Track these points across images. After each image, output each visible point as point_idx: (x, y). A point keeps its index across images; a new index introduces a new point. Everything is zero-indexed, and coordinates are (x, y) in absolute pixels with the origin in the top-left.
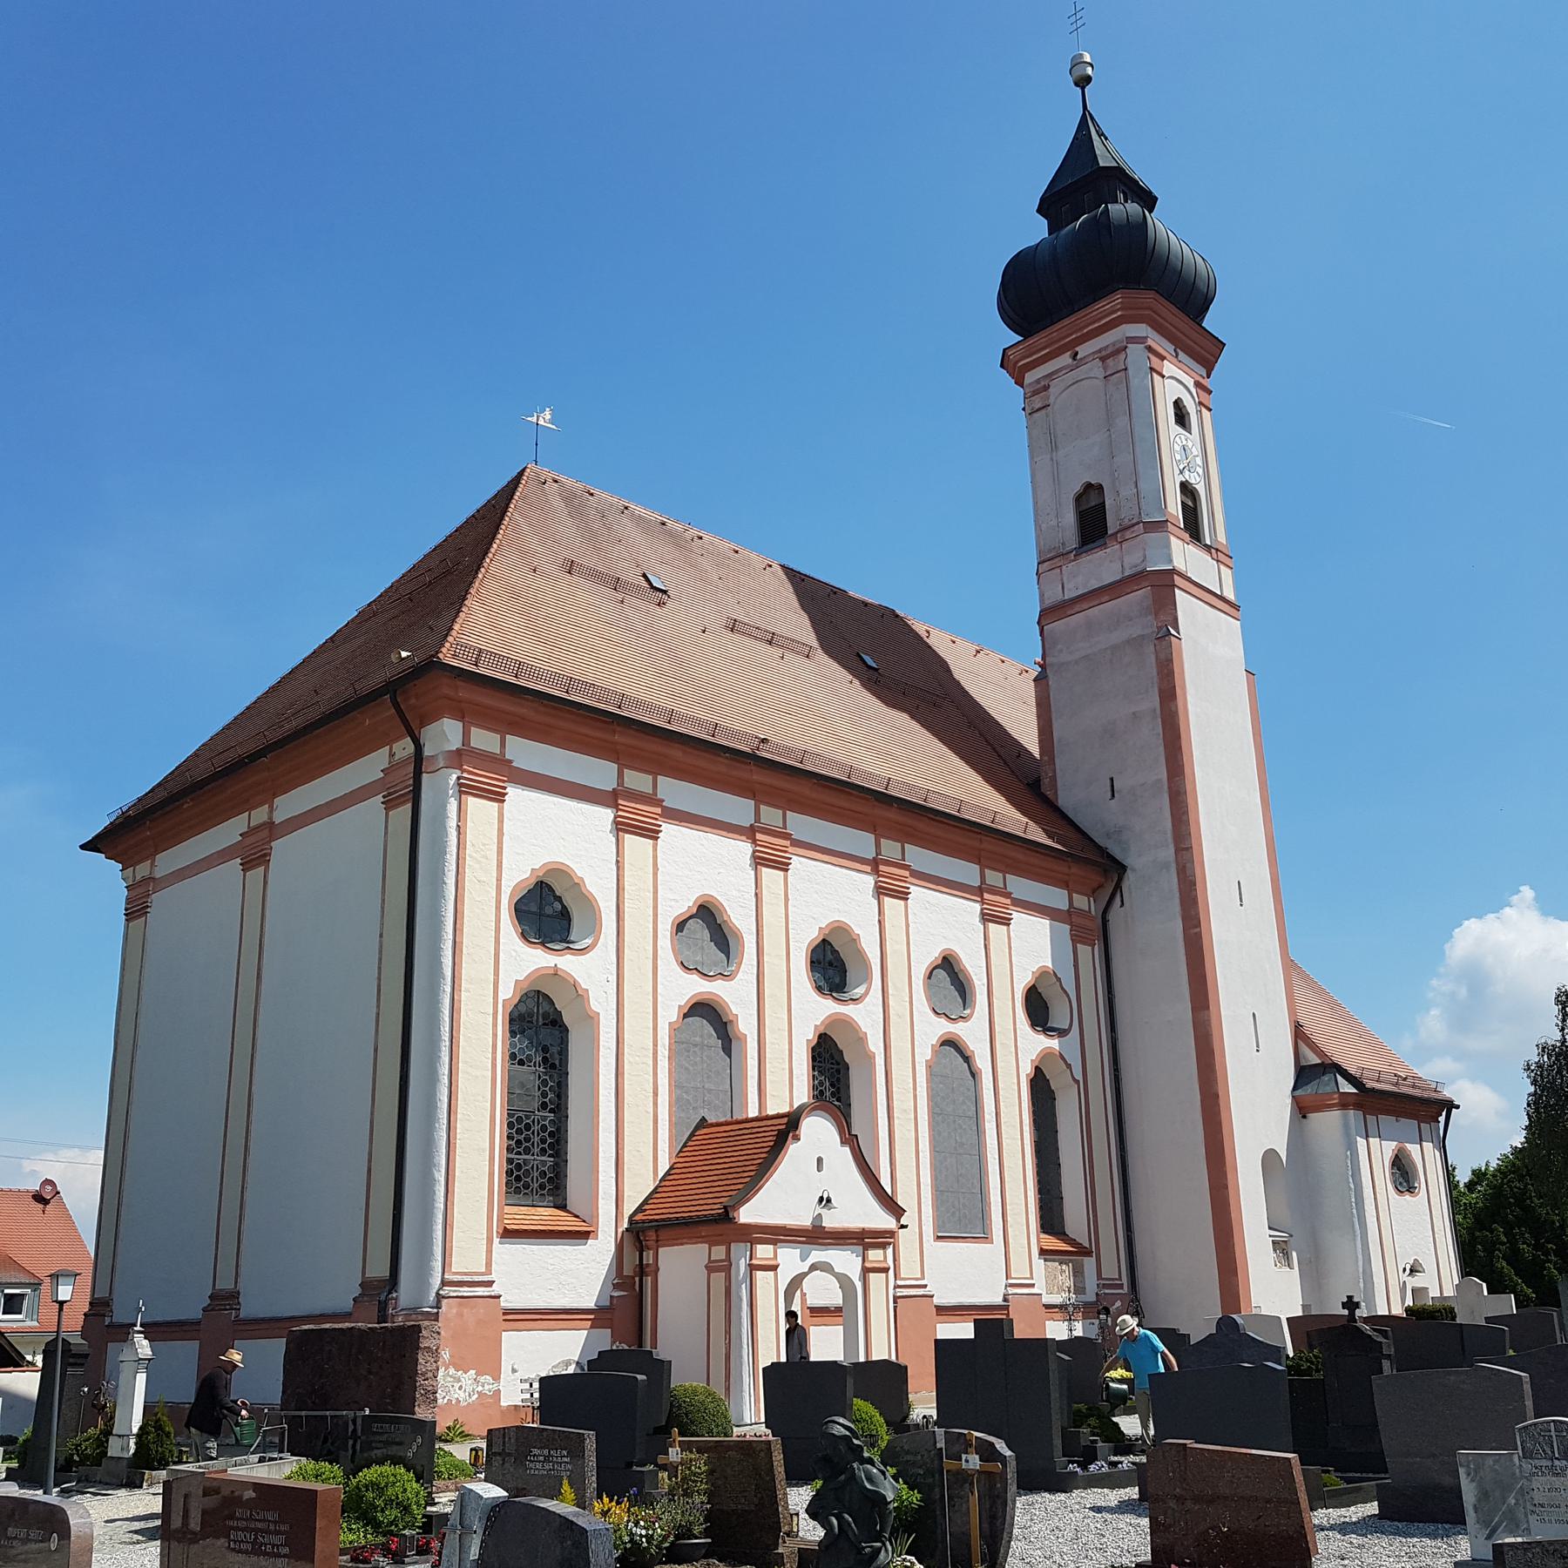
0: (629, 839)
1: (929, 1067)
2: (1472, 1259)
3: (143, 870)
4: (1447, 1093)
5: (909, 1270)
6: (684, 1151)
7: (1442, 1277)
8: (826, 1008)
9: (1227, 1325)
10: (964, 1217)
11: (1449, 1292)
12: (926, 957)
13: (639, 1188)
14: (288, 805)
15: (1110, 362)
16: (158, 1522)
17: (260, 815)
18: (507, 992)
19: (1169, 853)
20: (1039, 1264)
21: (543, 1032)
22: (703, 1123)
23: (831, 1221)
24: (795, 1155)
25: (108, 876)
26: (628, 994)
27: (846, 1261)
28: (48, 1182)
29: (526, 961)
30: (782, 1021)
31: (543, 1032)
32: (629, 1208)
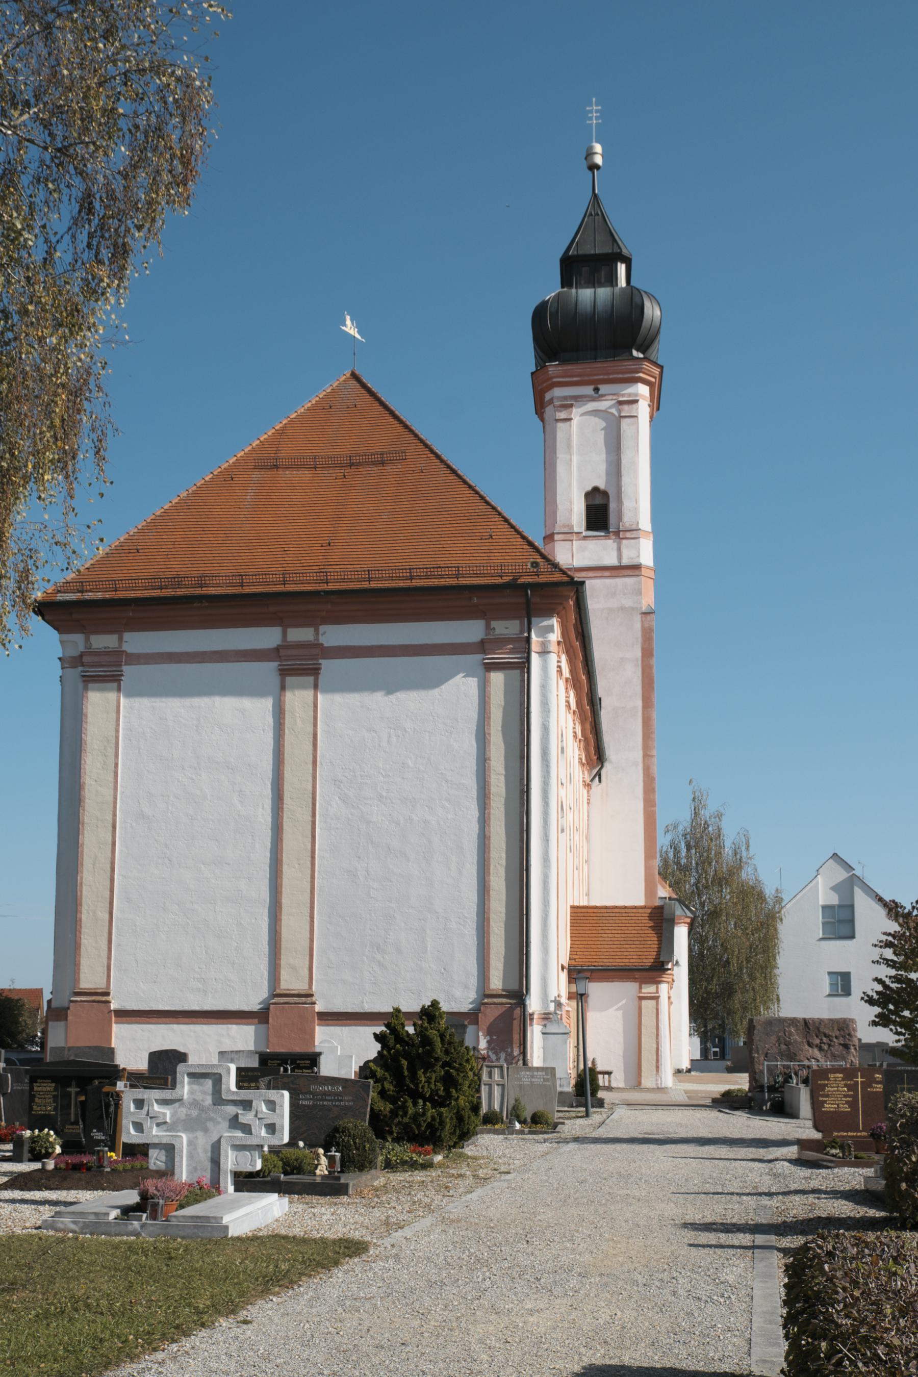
14: (334, 635)
15: (626, 407)
17: (300, 634)
19: (638, 755)
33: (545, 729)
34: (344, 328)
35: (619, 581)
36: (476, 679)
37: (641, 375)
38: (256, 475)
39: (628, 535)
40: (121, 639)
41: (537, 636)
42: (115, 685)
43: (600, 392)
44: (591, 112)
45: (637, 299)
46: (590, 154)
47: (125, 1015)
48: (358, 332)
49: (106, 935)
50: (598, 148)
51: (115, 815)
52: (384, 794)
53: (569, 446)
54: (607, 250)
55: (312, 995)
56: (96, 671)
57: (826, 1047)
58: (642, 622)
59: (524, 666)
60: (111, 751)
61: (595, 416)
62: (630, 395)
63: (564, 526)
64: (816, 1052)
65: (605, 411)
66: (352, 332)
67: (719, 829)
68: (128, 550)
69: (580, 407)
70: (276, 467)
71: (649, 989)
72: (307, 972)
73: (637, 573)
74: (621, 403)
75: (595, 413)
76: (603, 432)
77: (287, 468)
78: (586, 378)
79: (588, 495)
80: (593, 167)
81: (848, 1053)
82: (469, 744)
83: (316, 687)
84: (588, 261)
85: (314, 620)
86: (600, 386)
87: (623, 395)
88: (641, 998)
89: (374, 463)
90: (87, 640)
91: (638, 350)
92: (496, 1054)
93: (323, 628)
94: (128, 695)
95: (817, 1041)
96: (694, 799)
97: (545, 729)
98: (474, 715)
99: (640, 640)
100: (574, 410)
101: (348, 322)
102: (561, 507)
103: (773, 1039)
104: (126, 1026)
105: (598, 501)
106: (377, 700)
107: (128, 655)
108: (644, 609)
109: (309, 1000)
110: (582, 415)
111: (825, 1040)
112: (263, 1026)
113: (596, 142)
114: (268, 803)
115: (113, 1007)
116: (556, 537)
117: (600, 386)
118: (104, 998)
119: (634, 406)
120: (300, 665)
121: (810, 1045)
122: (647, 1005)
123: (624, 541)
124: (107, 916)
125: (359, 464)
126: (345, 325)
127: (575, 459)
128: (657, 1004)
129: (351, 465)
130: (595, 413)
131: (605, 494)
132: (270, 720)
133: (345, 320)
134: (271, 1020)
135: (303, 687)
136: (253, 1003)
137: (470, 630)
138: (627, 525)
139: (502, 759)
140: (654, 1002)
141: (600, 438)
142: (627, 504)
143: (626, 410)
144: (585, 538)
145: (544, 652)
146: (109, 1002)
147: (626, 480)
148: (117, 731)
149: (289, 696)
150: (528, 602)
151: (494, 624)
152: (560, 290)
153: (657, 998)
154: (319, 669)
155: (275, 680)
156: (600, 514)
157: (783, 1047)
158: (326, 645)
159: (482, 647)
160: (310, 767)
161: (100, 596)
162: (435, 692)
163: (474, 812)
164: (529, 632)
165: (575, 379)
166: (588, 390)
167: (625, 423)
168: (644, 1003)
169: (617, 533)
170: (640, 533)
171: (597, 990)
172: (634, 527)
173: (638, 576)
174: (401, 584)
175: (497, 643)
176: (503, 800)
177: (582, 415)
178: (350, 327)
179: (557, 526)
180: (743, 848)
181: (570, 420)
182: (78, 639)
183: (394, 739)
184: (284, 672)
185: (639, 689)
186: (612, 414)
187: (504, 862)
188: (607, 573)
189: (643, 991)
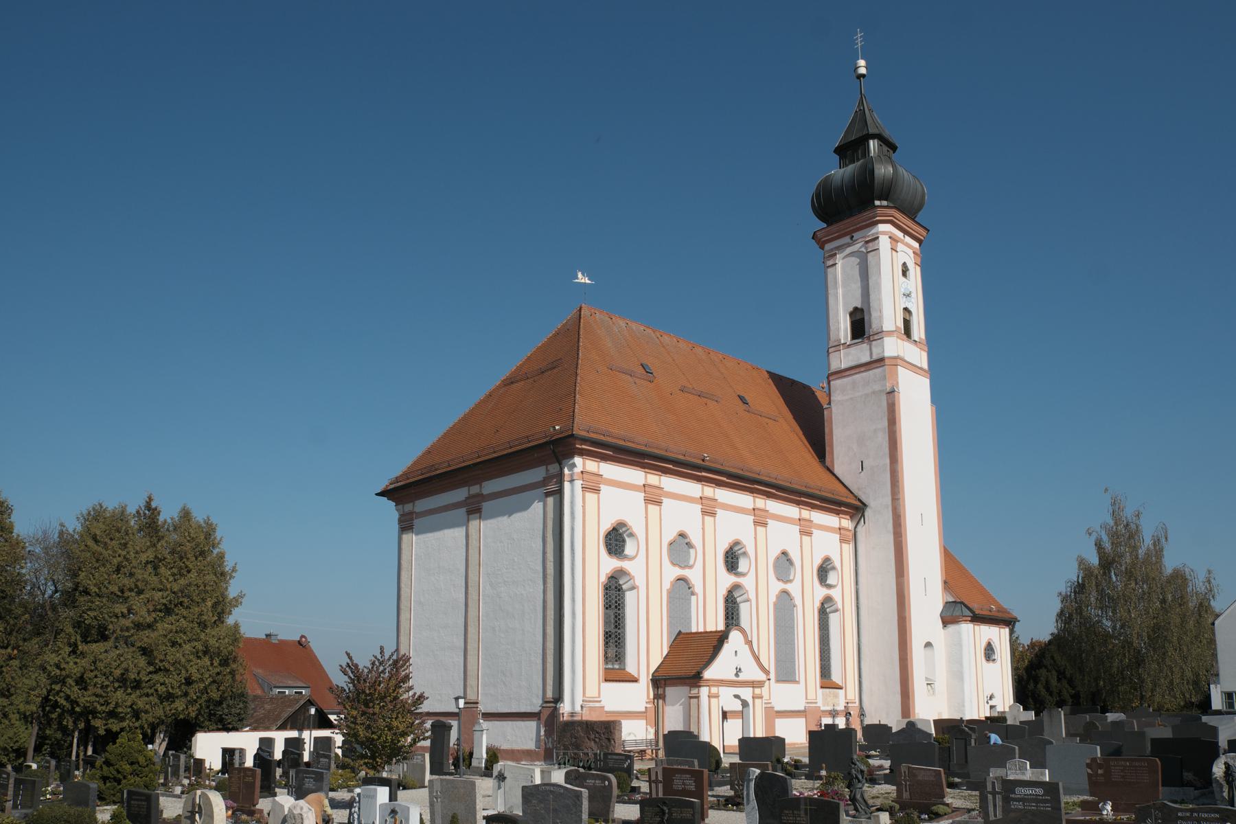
0: (650, 507)
1: (775, 605)
2: (1023, 694)
3: (408, 507)
4: (1015, 614)
5: (766, 696)
6: (672, 647)
7: (1005, 700)
8: (731, 579)
9: (911, 725)
10: (787, 674)
11: (1007, 709)
12: (775, 553)
13: (656, 661)
14: (490, 487)
16: (237, 765)
17: (475, 489)
18: (603, 579)
19: (888, 500)
20: (820, 691)
21: (614, 594)
22: (680, 632)
23: (742, 677)
24: (727, 649)
25: (389, 505)
26: (649, 574)
27: (746, 693)
28: (303, 636)
29: (610, 564)
30: (711, 583)
31: (614, 594)
32: (652, 670)
33: (573, 529)
50: (862, 63)
53: (836, 283)
56: (406, 525)
59: (559, 492)
71: (694, 691)
74: (867, 242)
75: (851, 254)
79: (851, 314)
84: (851, 149)
85: (478, 480)
91: (880, 199)
93: (484, 484)
94: (417, 534)
97: (573, 529)
101: (580, 275)
102: (832, 328)
105: (858, 317)
106: (504, 520)
120: (474, 508)
122: (694, 701)
127: (840, 291)
131: (862, 310)
137: (537, 474)
141: (856, 272)
142: (874, 314)
143: (871, 246)
145: (572, 481)
153: (698, 697)
159: (544, 482)
166: (847, 239)
169: (868, 338)
171: (671, 691)
175: (544, 482)
178: (582, 279)
184: (470, 513)
185: (887, 450)
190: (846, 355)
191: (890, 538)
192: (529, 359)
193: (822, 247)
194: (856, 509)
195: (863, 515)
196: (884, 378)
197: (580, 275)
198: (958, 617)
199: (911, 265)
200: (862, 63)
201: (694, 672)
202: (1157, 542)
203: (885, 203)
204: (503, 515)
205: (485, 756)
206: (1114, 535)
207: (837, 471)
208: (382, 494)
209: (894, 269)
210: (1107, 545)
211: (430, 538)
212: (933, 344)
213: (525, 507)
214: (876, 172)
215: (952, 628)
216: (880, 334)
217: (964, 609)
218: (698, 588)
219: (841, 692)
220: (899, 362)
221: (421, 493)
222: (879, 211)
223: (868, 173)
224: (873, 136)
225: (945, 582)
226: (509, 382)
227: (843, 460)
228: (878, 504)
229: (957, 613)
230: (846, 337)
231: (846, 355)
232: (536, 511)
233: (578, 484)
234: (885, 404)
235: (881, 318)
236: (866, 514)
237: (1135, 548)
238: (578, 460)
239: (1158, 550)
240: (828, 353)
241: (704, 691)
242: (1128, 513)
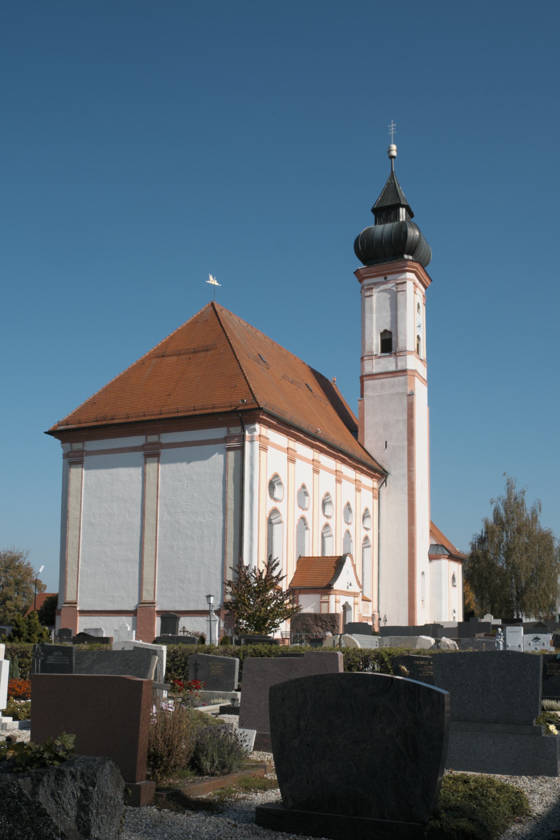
14: (166, 438)
15: (400, 286)
17: (153, 438)
19: (405, 471)
32: (289, 583)
33: (252, 477)
34: (208, 282)
35: (396, 379)
36: (223, 455)
37: (407, 268)
38: (154, 361)
39: (401, 354)
40: (83, 445)
41: (249, 433)
42: (81, 465)
43: (388, 279)
44: (391, 128)
45: (404, 229)
46: (389, 151)
47: (84, 613)
48: (217, 282)
49: (76, 577)
50: (394, 147)
51: (80, 524)
52: (185, 510)
53: (371, 310)
54: (393, 202)
55: (154, 603)
56: (74, 459)
57: (324, 626)
58: (408, 400)
59: (242, 448)
60: (79, 495)
61: (385, 292)
62: (402, 279)
63: (369, 352)
64: (320, 629)
65: (390, 289)
66: (213, 283)
67: (523, 500)
68: (92, 403)
69: (377, 288)
70: (164, 356)
71: (325, 598)
72: (153, 592)
73: (405, 374)
74: (398, 284)
75: (385, 290)
76: (389, 300)
77: (168, 356)
78: (379, 273)
79: (382, 334)
80: (392, 157)
81: (335, 629)
82: (219, 485)
83: (158, 462)
84: (385, 211)
85: (158, 432)
86: (387, 276)
87: (399, 280)
88: (322, 602)
89: (204, 351)
90: (71, 446)
91: (408, 254)
92: (227, 629)
93: (162, 435)
94: (87, 469)
95: (320, 624)
96: (508, 484)
97: (252, 477)
98: (222, 472)
99: (406, 410)
100: (374, 290)
101: (211, 278)
103: (300, 623)
104: (84, 617)
105: (387, 337)
106: (183, 466)
107: (86, 451)
108: (409, 393)
109: (153, 605)
110: (378, 292)
111: (324, 623)
112: (135, 617)
113: (394, 144)
114: (139, 516)
115: (78, 609)
116: (365, 358)
117: (387, 276)
118: (74, 605)
119: (404, 285)
120: (152, 453)
121: (317, 625)
123: (399, 358)
124: (77, 569)
125: (198, 352)
126: (209, 280)
127: (374, 316)
128: (328, 605)
129: (195, 352)
130: (385, 290)
131: (390, 333)
132: (140, 478)
133: (209, 277)
134: (138, 614)
135: (153, 462)
136: (131, 605)
137: (220, 433)
138: (400, 349)
139: (233, 492)
140: (326, 604)
141: (387, 304)
142: (401, 337)
143: (400, 287)
144: (380, 357)
145: (252, 441)
146: (76, 607)
147: (400, 324)
148: (82, 486)
149: (148, 466)
150: (241, 419)
151: (231, 429)
152: (372, 226)
153: (328, 602)
154: (159, 454)
155: (143, 459)
156: (388, 344)
157: (305, 626)
158: (163, 443)
159: (226, 440)
160: (156, 499)
161: (74, 426)
162: (206, 462)
163: (221, 517)
164: (244, 431)
165: (374, 274)
166: (381, 279)
167: (400, 295)
168: (323, 604)
169: (395, 354)
170: (407, 353)
172: (404, 350)
173: (406, 375)
174: (190, 413)
175: (226, 440)
176: (233, 511)
177: (378, 292)
178: (212, 281)
179: (365, 352)
180: (538, 510)
181: (371, 296)
182: (68, 445)
183: (189, 485)
184: (146, 456)
185: (405, 435)
186: (393, 290)
187: (232, 540)
188: (390, 375)
189: (323, 598)
190: (377, 363)
191: (406, 498)
192: (172, 338)
193: (361, 281)
194: (380, 473)
195: (385, 481)
196: (406, 384)
197: (211, 278)
198: (440, 555)
199: (421, 305)
200: (394, 147)
201: (324, 585)
202: (534, 512)
203: (411, 258)
204: (182, 461)
205: (217, 639)
206: (507, 505)
207: (367, 446)
208: (50, 433)
209: (410, 305)
210: (502, 512)
211: (103, 474)
212: (430, 362)
213: (206, 457)
214: (409, 234)
215: (435, 562)
216: (404, 352)
217: (444, 550)
218: (310, 526)
219: (370, 603)
220: (416, 373)
221: (81, 437)
222: (409, 263)
223: (402, 231)
224: (403, 206)
225: (431, 531)
226: (160, 354)
227: (372, 441)
228: (397, 473)
229: (441, 552)
230: (377, 350)
231: (377, 363)
232: (216, 462)
233: (257, 444)
234: (405, 403)
235: (405, 340)
236: (388, 480)
237: (521, 515)
238: (257, 426)
239: (535, 519)
240: (362, 359)
241: (332, 598)
242: (517, 491)
